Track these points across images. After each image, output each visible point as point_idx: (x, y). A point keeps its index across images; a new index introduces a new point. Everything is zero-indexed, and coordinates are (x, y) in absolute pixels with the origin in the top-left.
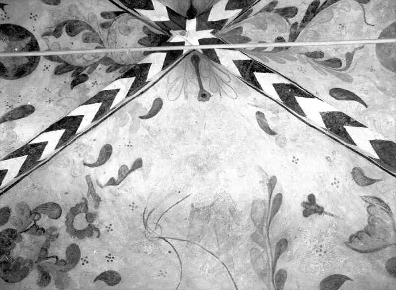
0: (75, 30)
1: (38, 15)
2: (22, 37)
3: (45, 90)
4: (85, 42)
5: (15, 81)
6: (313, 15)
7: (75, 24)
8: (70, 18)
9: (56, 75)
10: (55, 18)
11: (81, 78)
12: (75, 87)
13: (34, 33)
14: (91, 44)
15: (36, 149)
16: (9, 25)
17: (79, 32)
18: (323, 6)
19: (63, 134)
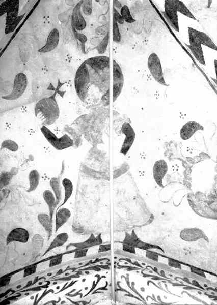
0: (80, 20)
1: (67, 54)
2: (86, 72)
3: (135, 49)
4: (91, 13)
5: (124, 78)
7: (75, 20)
8: (70, 23)
9: (121, 40)
10: (70, 39)
11: (125, 12)
12: (133, 17)
13: (83, 60)
14: (93, 6)
15: (195, 37)
16: (75, 82)
17: (82, 17)
19: (182, 13)
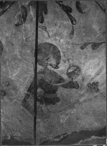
6: (65, 10)
18: (69, 15)
